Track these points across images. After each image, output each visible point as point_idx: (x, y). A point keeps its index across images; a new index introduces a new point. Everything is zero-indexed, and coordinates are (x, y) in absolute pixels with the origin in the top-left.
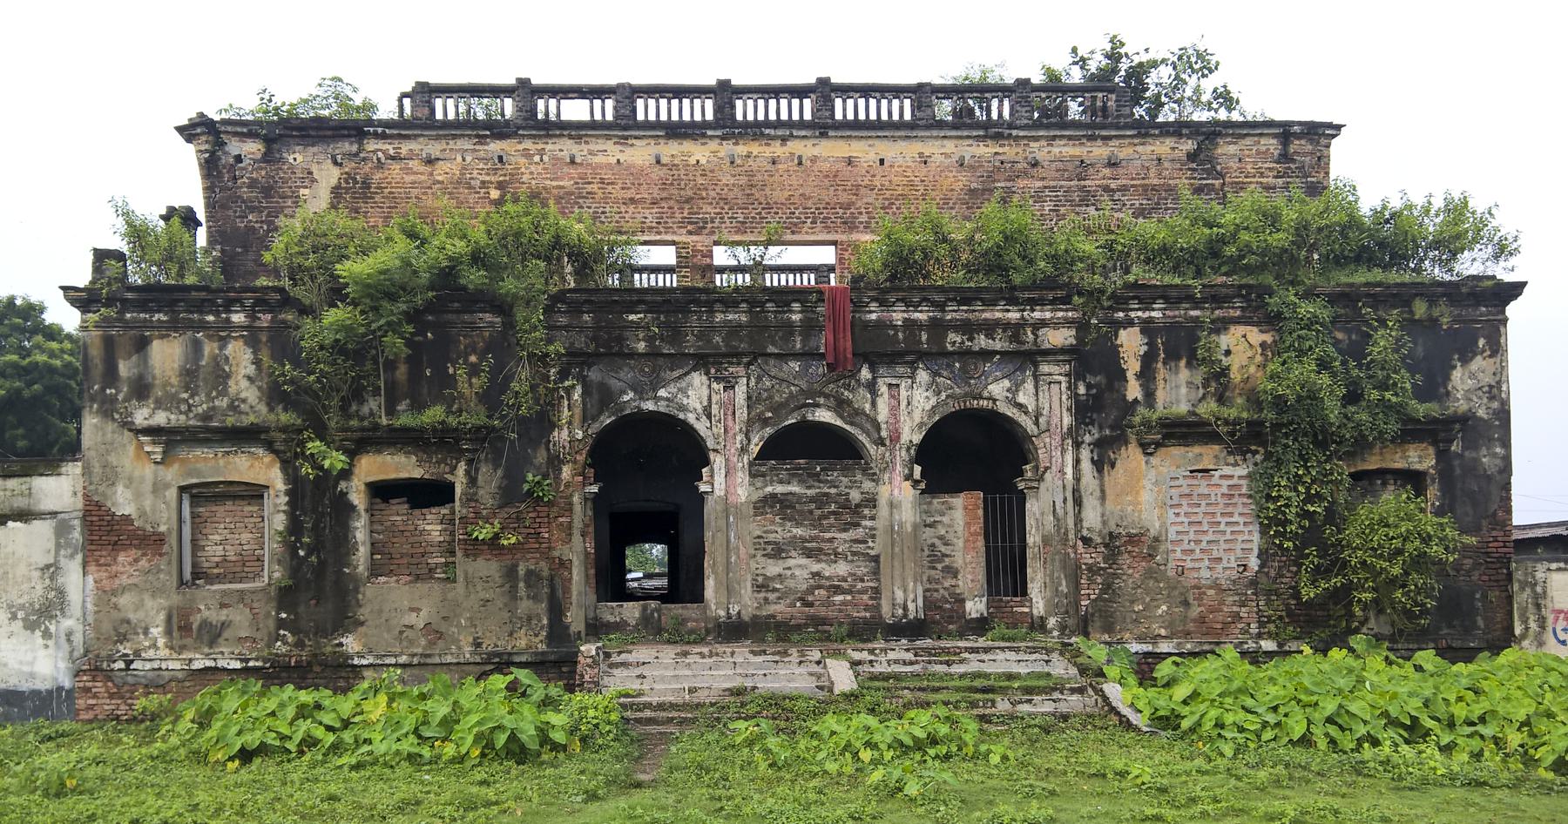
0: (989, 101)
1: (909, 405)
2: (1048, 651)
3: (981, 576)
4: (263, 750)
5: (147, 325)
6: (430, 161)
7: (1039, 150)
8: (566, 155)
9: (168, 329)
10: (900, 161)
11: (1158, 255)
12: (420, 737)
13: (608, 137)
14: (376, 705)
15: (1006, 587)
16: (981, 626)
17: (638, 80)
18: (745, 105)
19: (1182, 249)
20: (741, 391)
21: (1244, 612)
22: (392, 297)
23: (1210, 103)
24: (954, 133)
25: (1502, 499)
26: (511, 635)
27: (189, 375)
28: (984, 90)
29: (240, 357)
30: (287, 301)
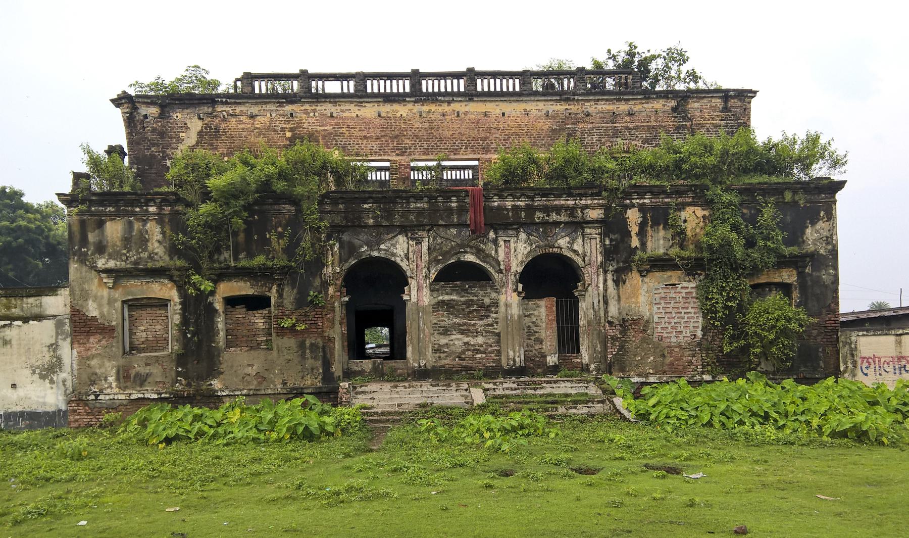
0: (562, 80)
1: (515, 251)
2: (588, 382)
3: (555, 343)
4: (177, 438)
6: (252, 117)
7: (590, 107)
8: (328, 112)
10: (513, 114)
11: (650, 169)
12: (258, 430)
13: (351, 102)
15: (573, 348)
16: (555, 370)
18: (427, 83)
20: (425, 245)
21: (694, 360)
22: (236, 197)
23: (685, 79)
24: (543, 98)
27: (127, 240)
28: (560, 74)
29: (154, 230)
30: (179, 200)
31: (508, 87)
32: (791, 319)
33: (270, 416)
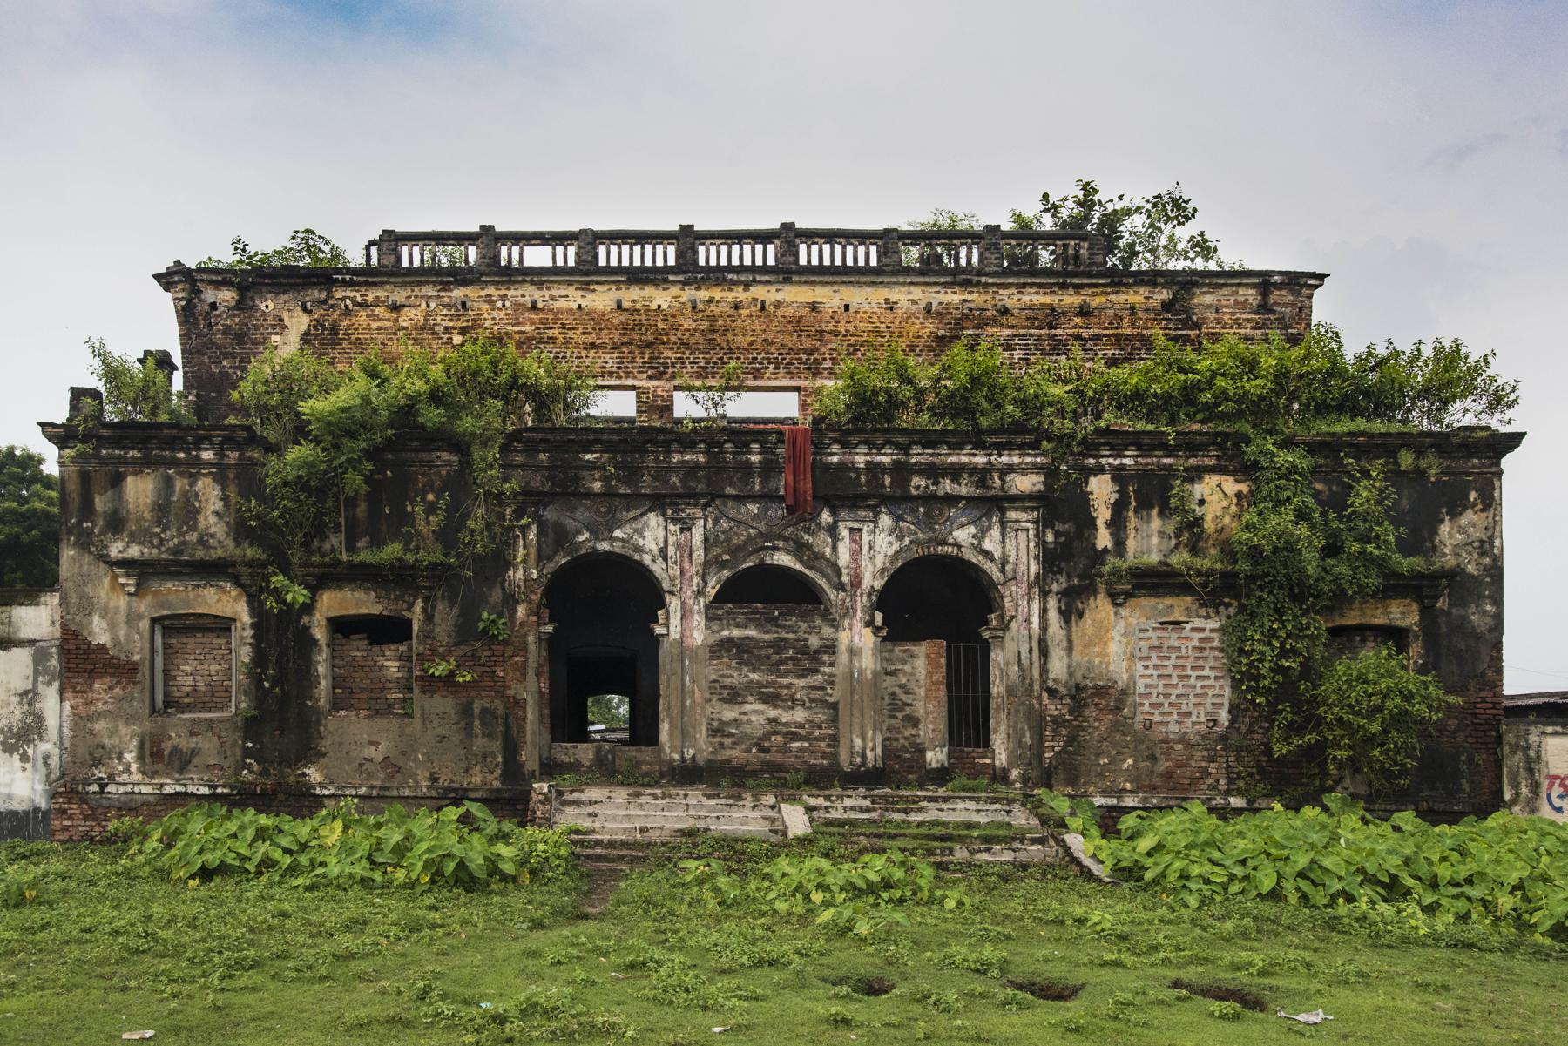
0: (957, 248)
1: (870, 549)
2: (1010, 802)
3: (943, 726)
4: (223, 869)
5: (121, 461)
6: (396, 308)
8: (527, 301)
9: (141, 465)
10: (866, 307)
11: (1131, 401)
12: (373, 862)
13: (570, 283)
14: (332, 830)
15: (968, 738)
16: (941, 776)
17: (598, 226)
19: (1155, 395)
22: (353, 435)
24: (921, 279)
25: (1492, 659)
26: (466, 771)
27: (161, 510)
28: (953, 236)
29: (209, 493)
30: (253, 439)
31: (855, 259)
32: (1412, 695)
33: (396, 838)
